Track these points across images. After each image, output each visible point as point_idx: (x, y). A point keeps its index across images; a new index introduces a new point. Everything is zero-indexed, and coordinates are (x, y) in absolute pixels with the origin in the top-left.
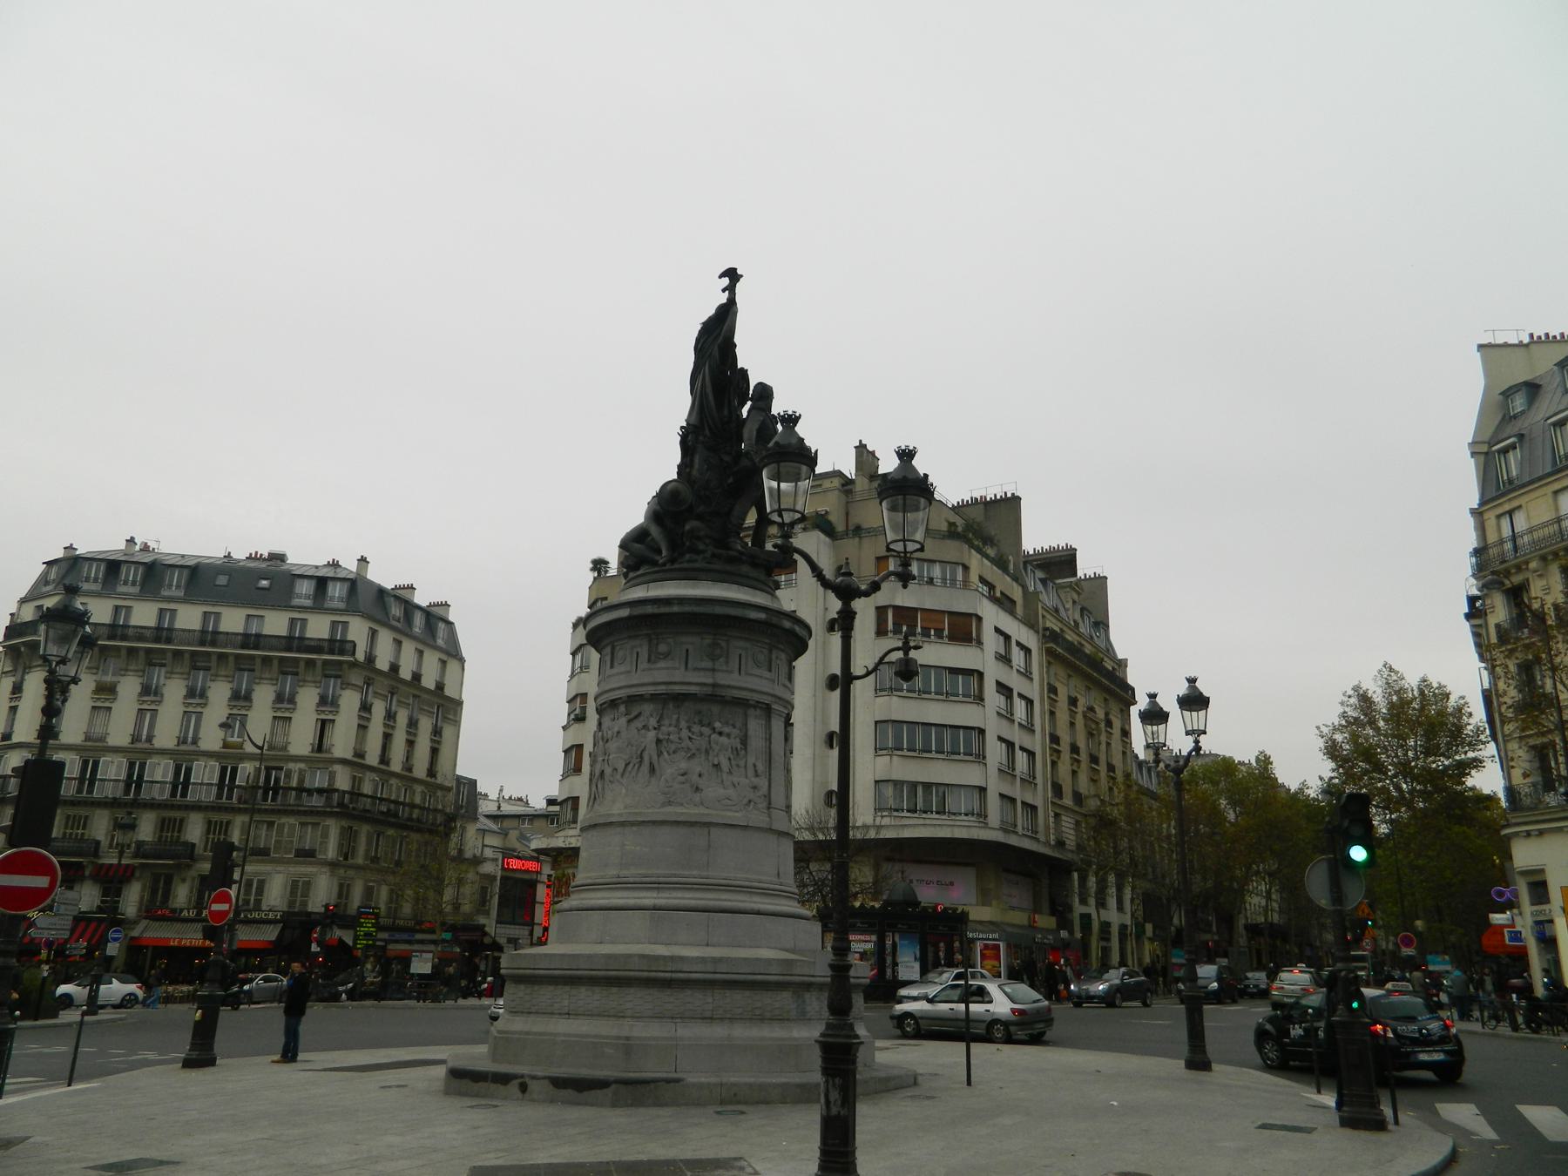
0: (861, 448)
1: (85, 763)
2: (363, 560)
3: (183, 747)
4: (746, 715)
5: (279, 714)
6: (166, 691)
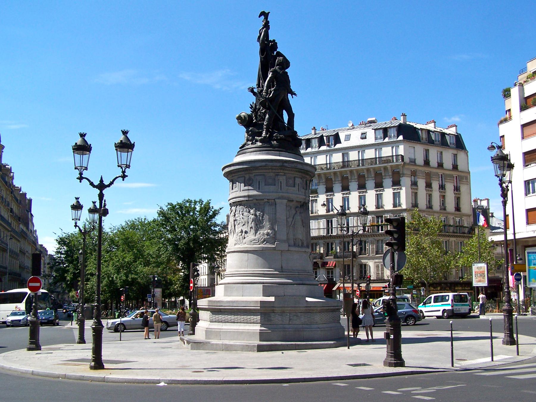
0: (259, 17)
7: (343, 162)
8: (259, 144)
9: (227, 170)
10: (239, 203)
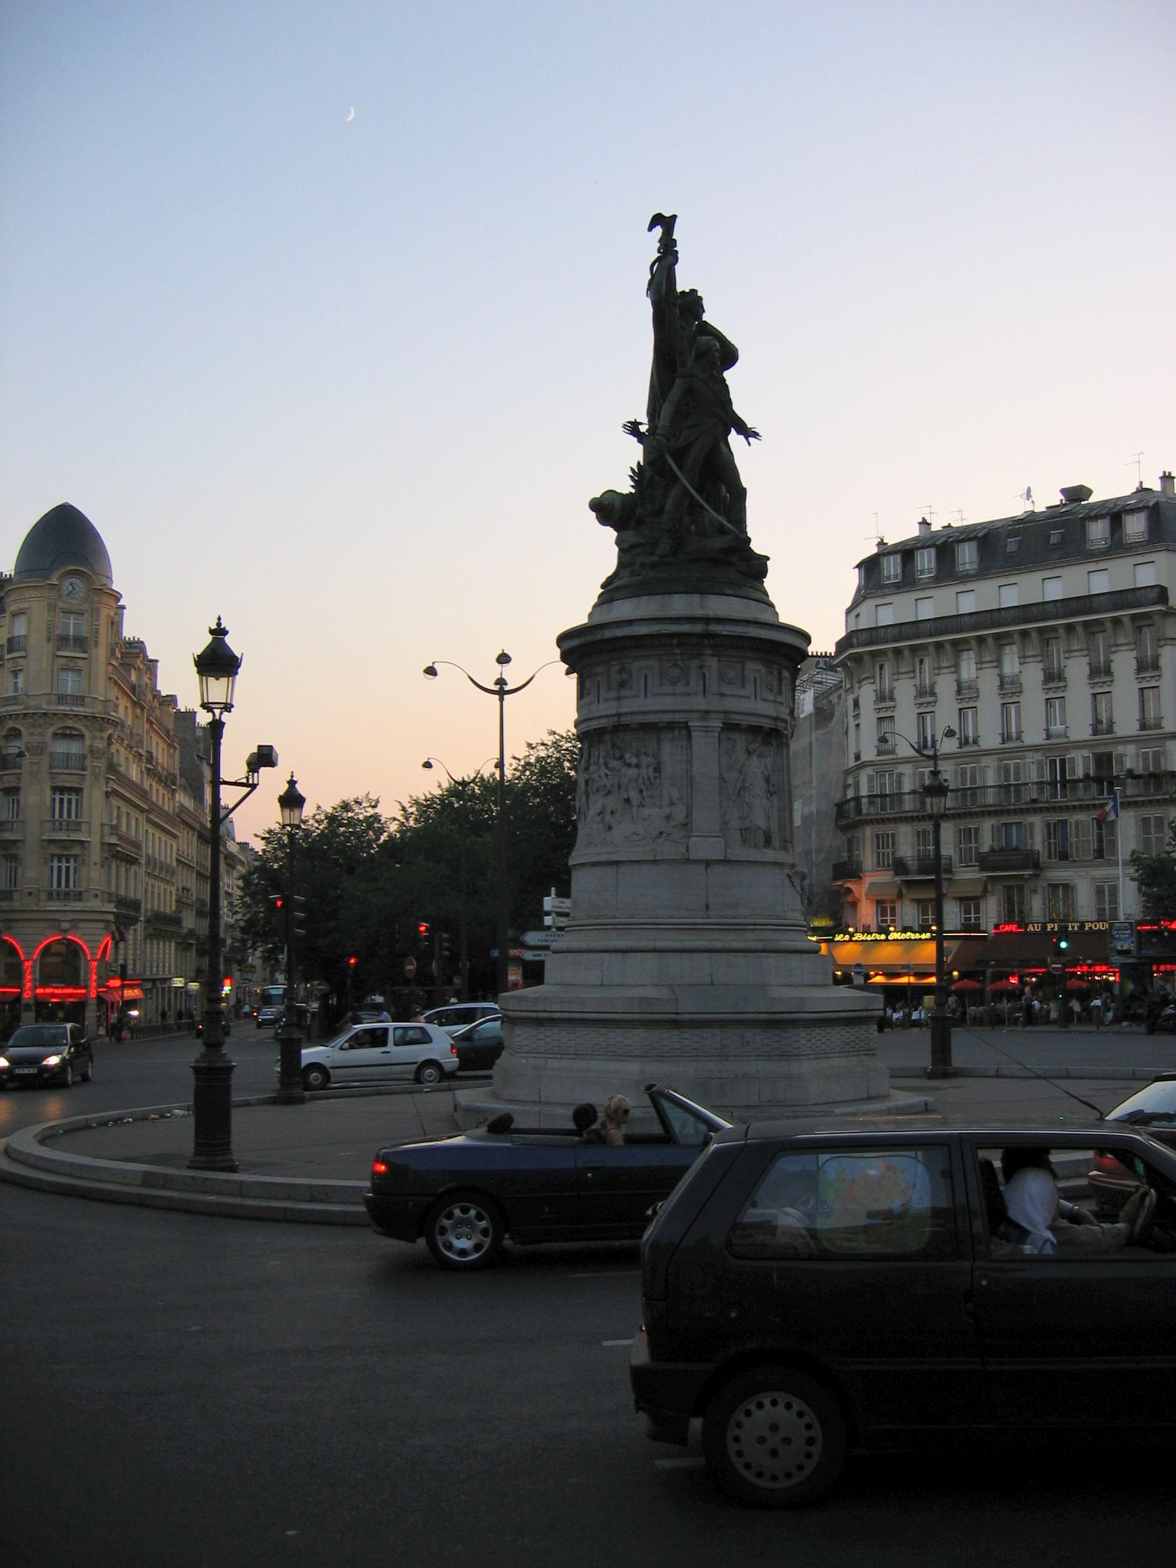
0: (650, 229)
1: (1053, 762)
4: (659, 741)
5: (882, 715)
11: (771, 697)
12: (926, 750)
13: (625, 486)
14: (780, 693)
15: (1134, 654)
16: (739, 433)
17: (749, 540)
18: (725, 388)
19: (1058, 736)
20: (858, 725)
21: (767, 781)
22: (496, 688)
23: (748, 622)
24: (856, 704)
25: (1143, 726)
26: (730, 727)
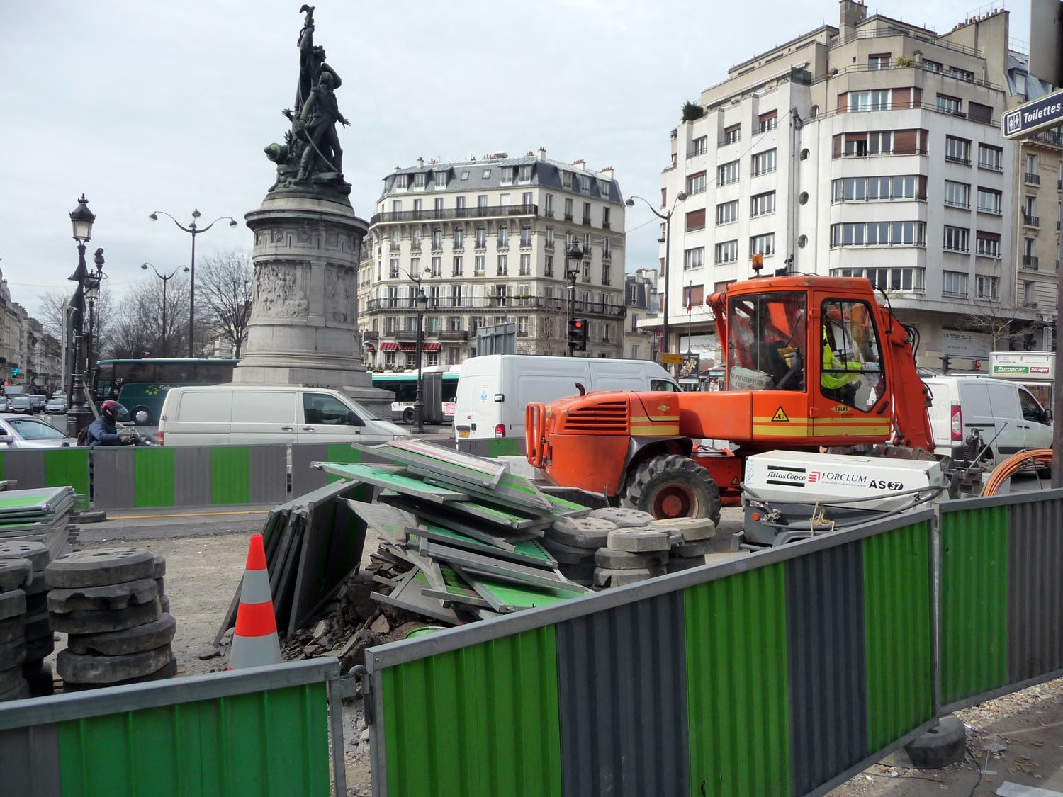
0: (301, 12)
2: (543, 150)
3: (456, 278)
6: (443, 246)
7: (458, 209)
8: (293, 187)
9: (251, 218)
10: (266, 263)
11: (350, 252)
12: (415, 280)
13: (283, 142)
14: (354, 250)
15: (520, 237)
16: (340, 121)
17: (343, 176)
18: (334, 95)
19: (481, 275)
20: (380, 262)
21: (346, 291)
22: (191, 229)
23: (341, 216)
24: (380, 251)
25: (522, 273)
26: (331, 264)
